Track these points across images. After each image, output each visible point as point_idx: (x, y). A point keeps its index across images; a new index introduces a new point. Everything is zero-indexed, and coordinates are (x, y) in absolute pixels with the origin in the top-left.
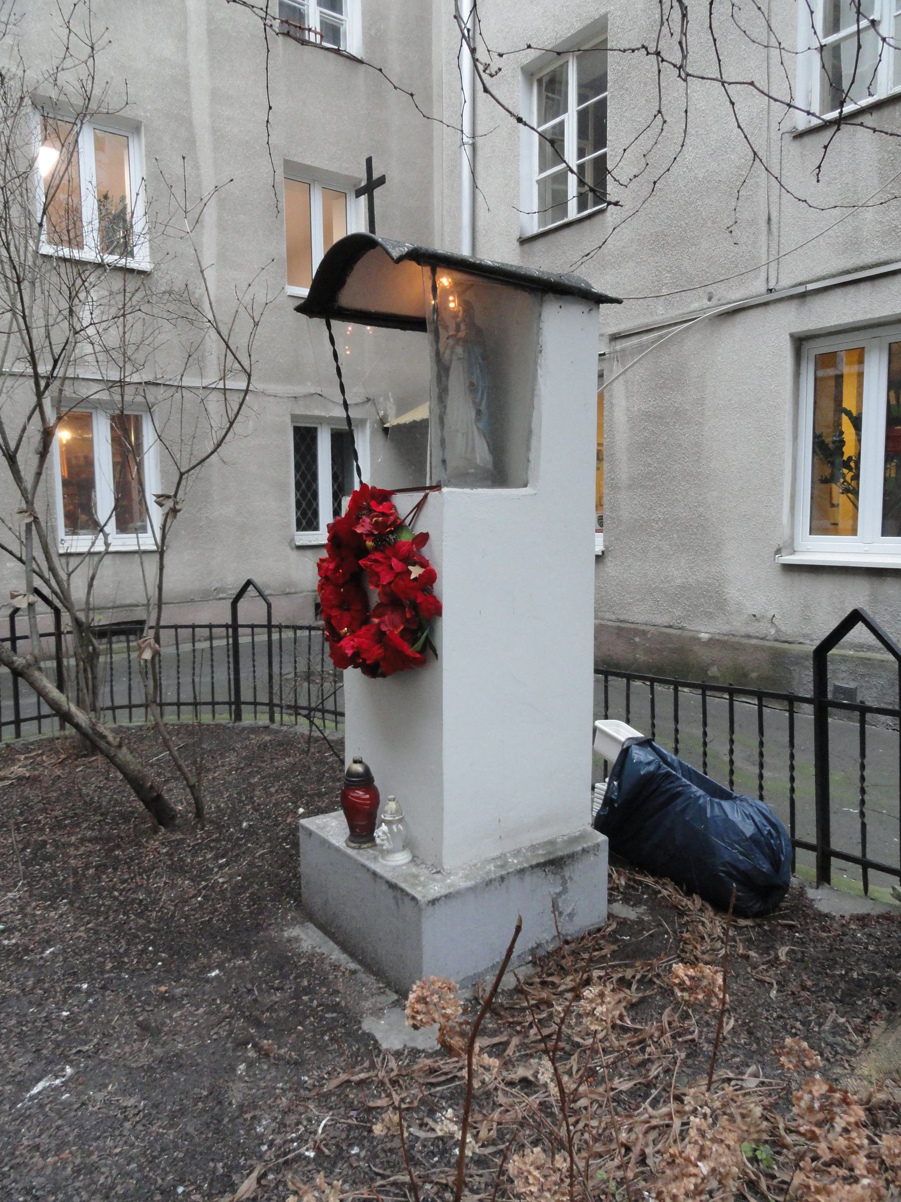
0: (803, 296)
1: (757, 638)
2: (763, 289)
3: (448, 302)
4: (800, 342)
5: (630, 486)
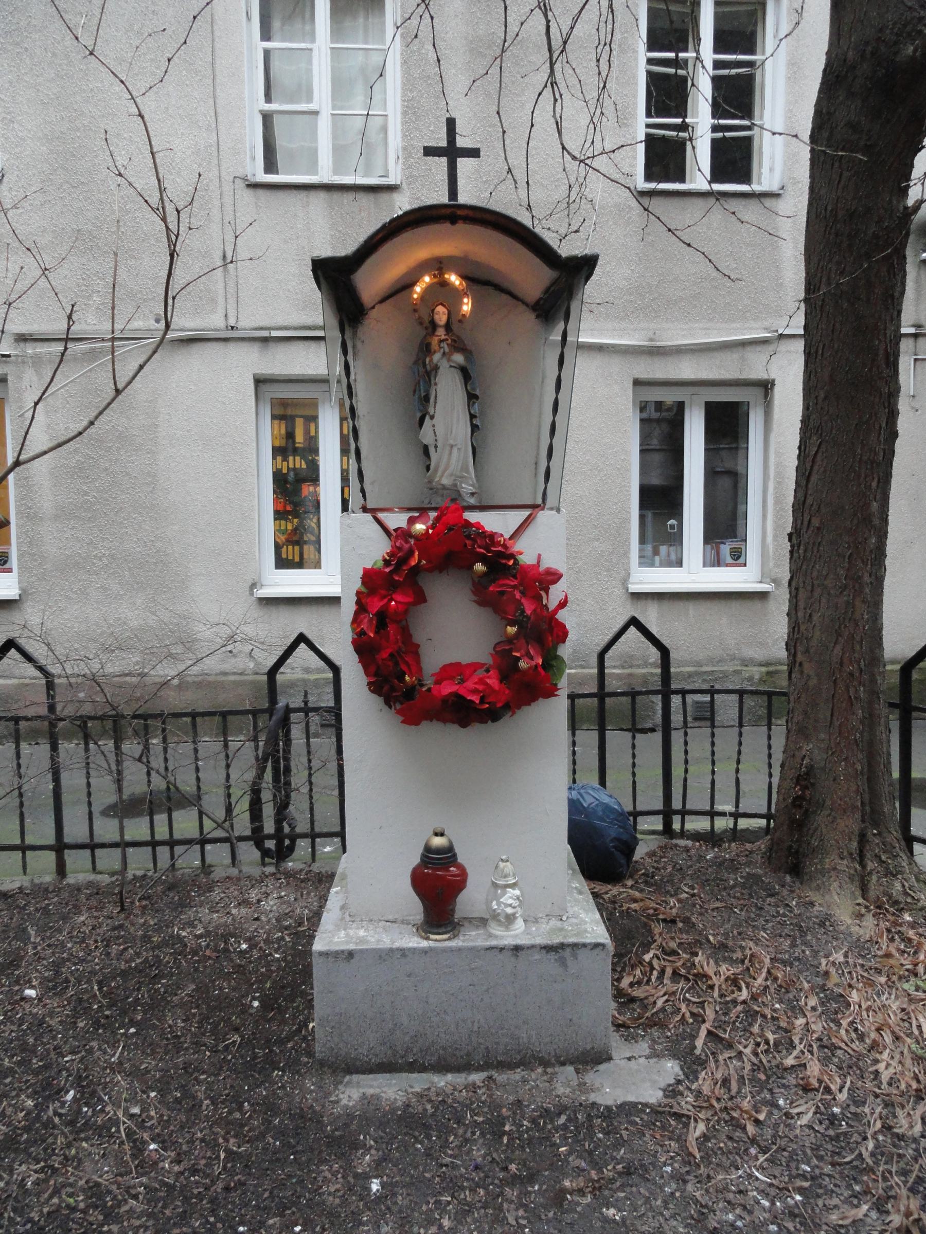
0: (265, 340)
1: (234, 674)
2: (221, 324)
3: (462, 303)
4: (260, 382)
5: (56, 518)
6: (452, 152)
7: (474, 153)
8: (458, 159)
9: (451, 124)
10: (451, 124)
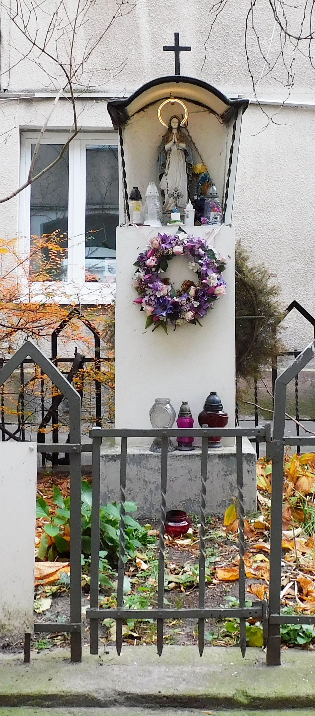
6: (177, 49)
7: (188, 49)
8: (180, 46)
9: (177, 36)
10: (177, 36)
